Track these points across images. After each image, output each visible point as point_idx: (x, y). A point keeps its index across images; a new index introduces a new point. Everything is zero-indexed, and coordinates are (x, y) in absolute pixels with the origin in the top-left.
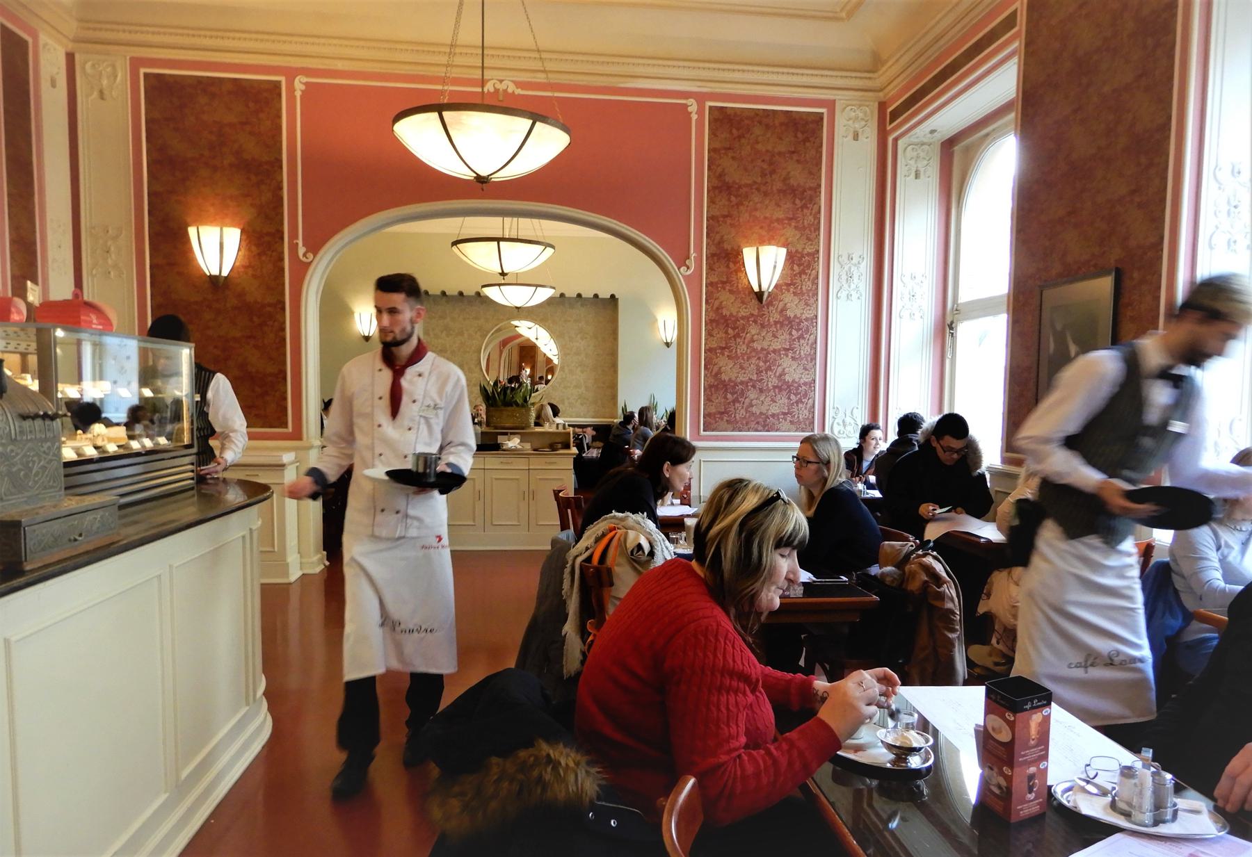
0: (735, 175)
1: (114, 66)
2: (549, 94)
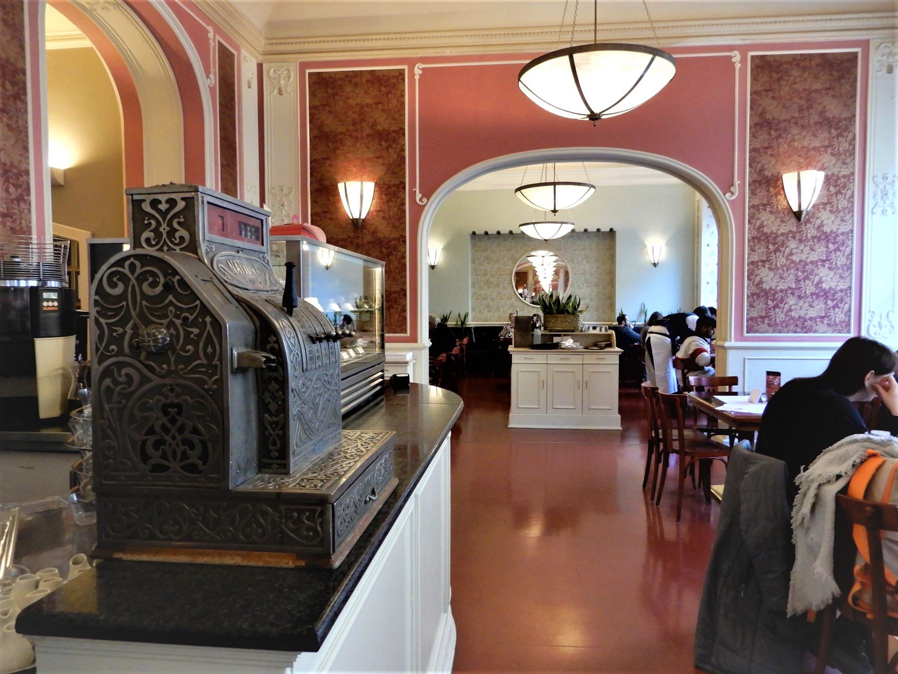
0: (774, 111)
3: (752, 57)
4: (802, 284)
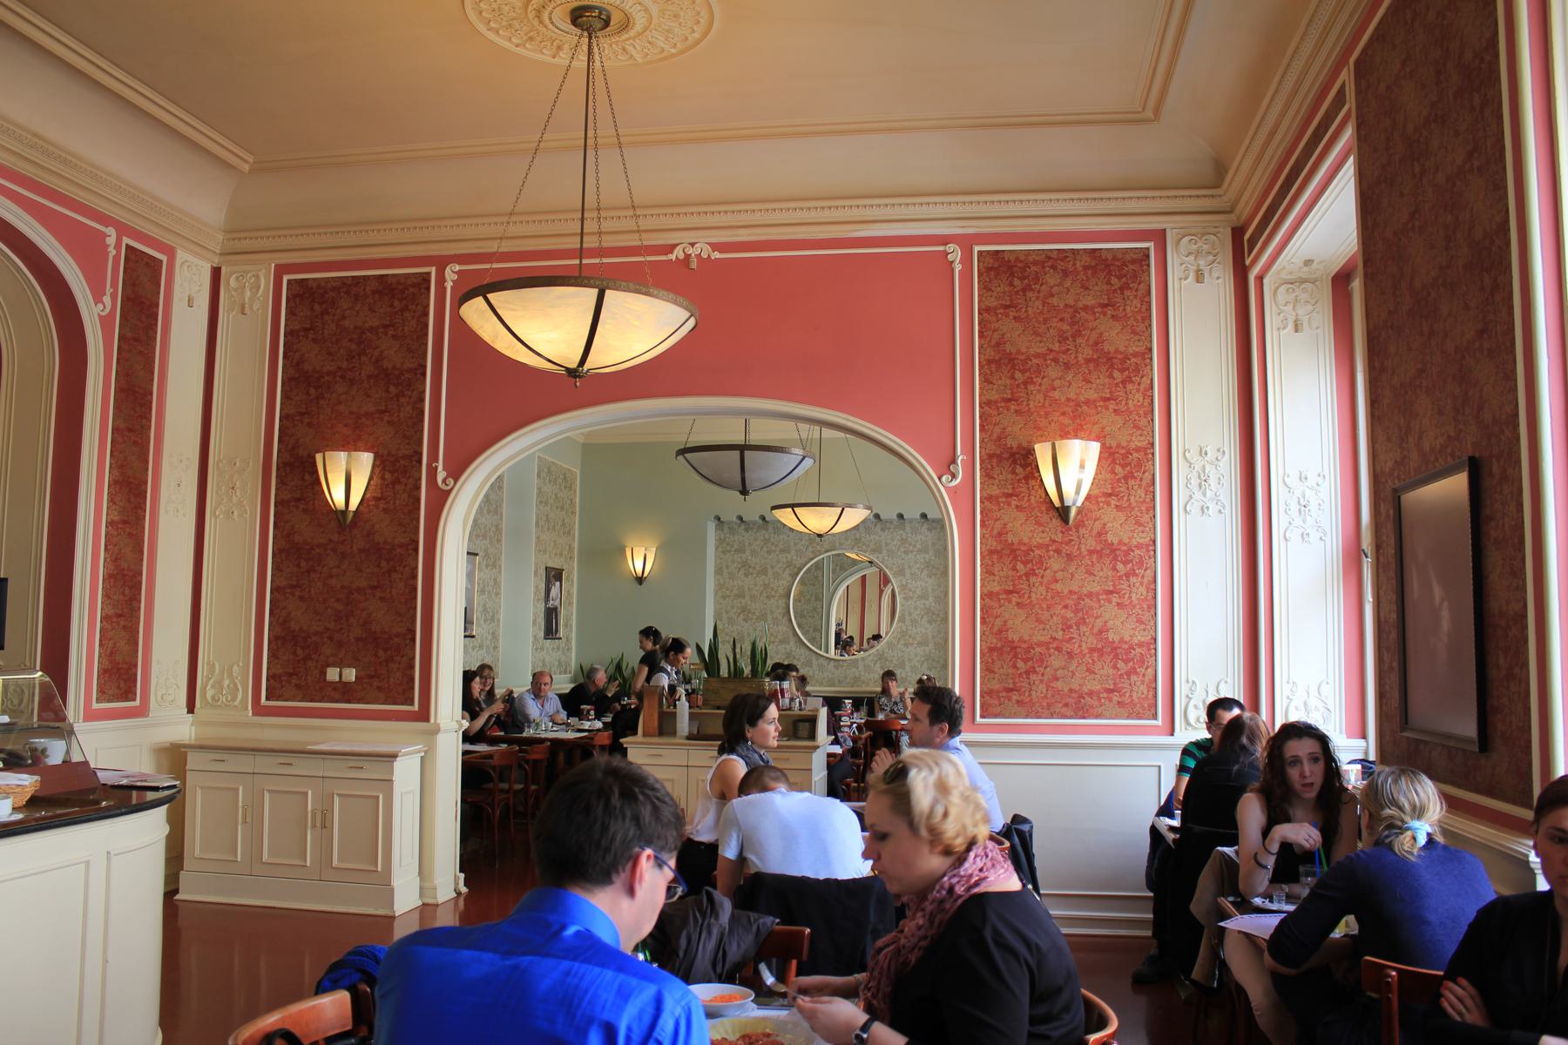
0: (1020, 341)
1: (257, 277)
4: (1074, 632)
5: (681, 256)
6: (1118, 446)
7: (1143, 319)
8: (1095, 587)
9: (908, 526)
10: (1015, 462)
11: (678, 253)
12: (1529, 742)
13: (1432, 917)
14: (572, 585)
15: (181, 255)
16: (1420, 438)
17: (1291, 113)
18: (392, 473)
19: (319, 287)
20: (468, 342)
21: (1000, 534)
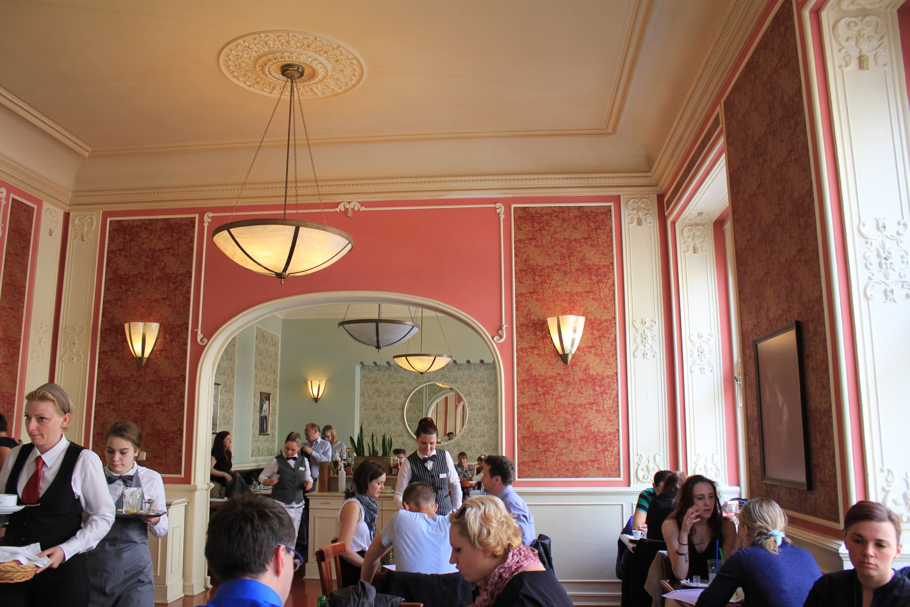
0: (538, 259)
1: (92, 219)
2: (320, 211)
3: (515, 208)
5: (343, 209)
6: (595, 319)
7: (608, 246)
8: (583, 401)
9: (472, 367)
10: (536, 328)
11: (341, 208)
12: (835, 483)
13: (786, 588)
14: (276, 401)
15: (46, 205)
16: (767, 311)
17: (693, 123)
18: (170, 335)
19: (129, 225)
20: (218, 257)
21: (528, 370)
